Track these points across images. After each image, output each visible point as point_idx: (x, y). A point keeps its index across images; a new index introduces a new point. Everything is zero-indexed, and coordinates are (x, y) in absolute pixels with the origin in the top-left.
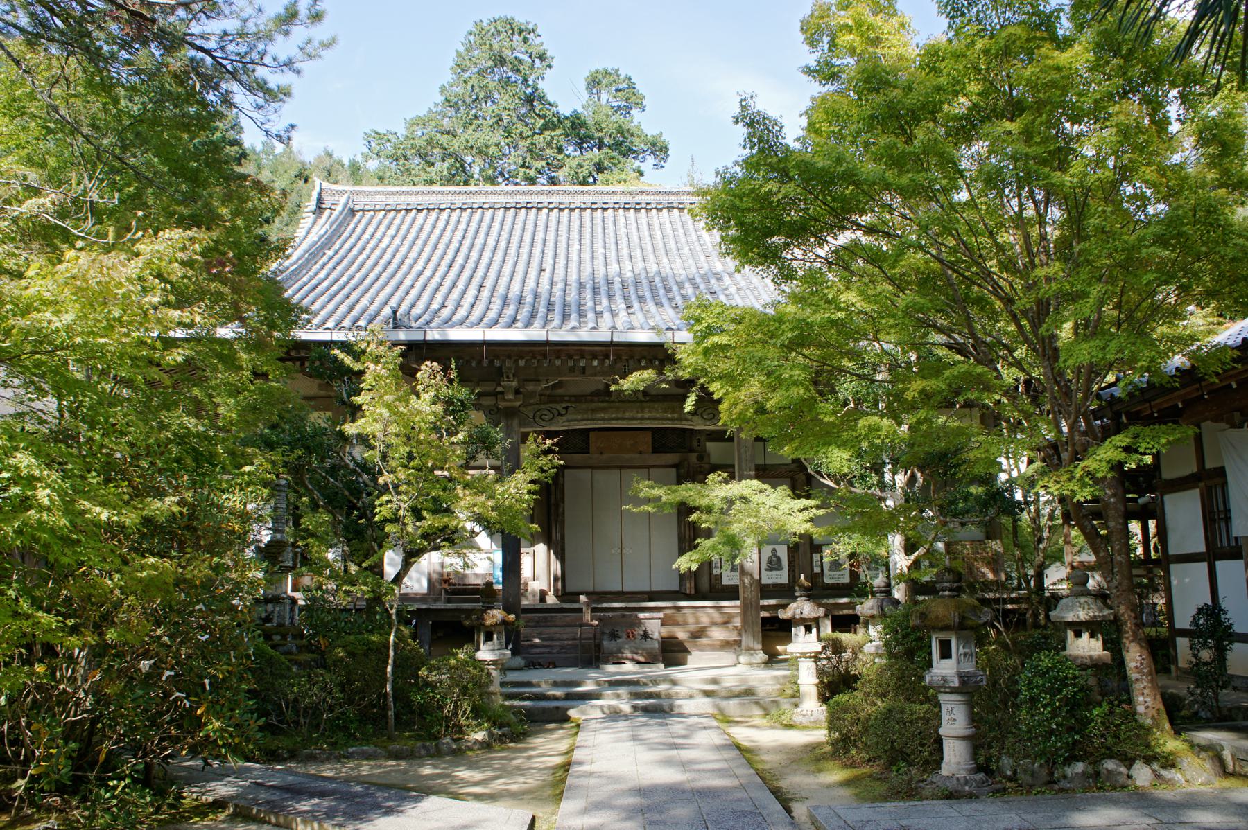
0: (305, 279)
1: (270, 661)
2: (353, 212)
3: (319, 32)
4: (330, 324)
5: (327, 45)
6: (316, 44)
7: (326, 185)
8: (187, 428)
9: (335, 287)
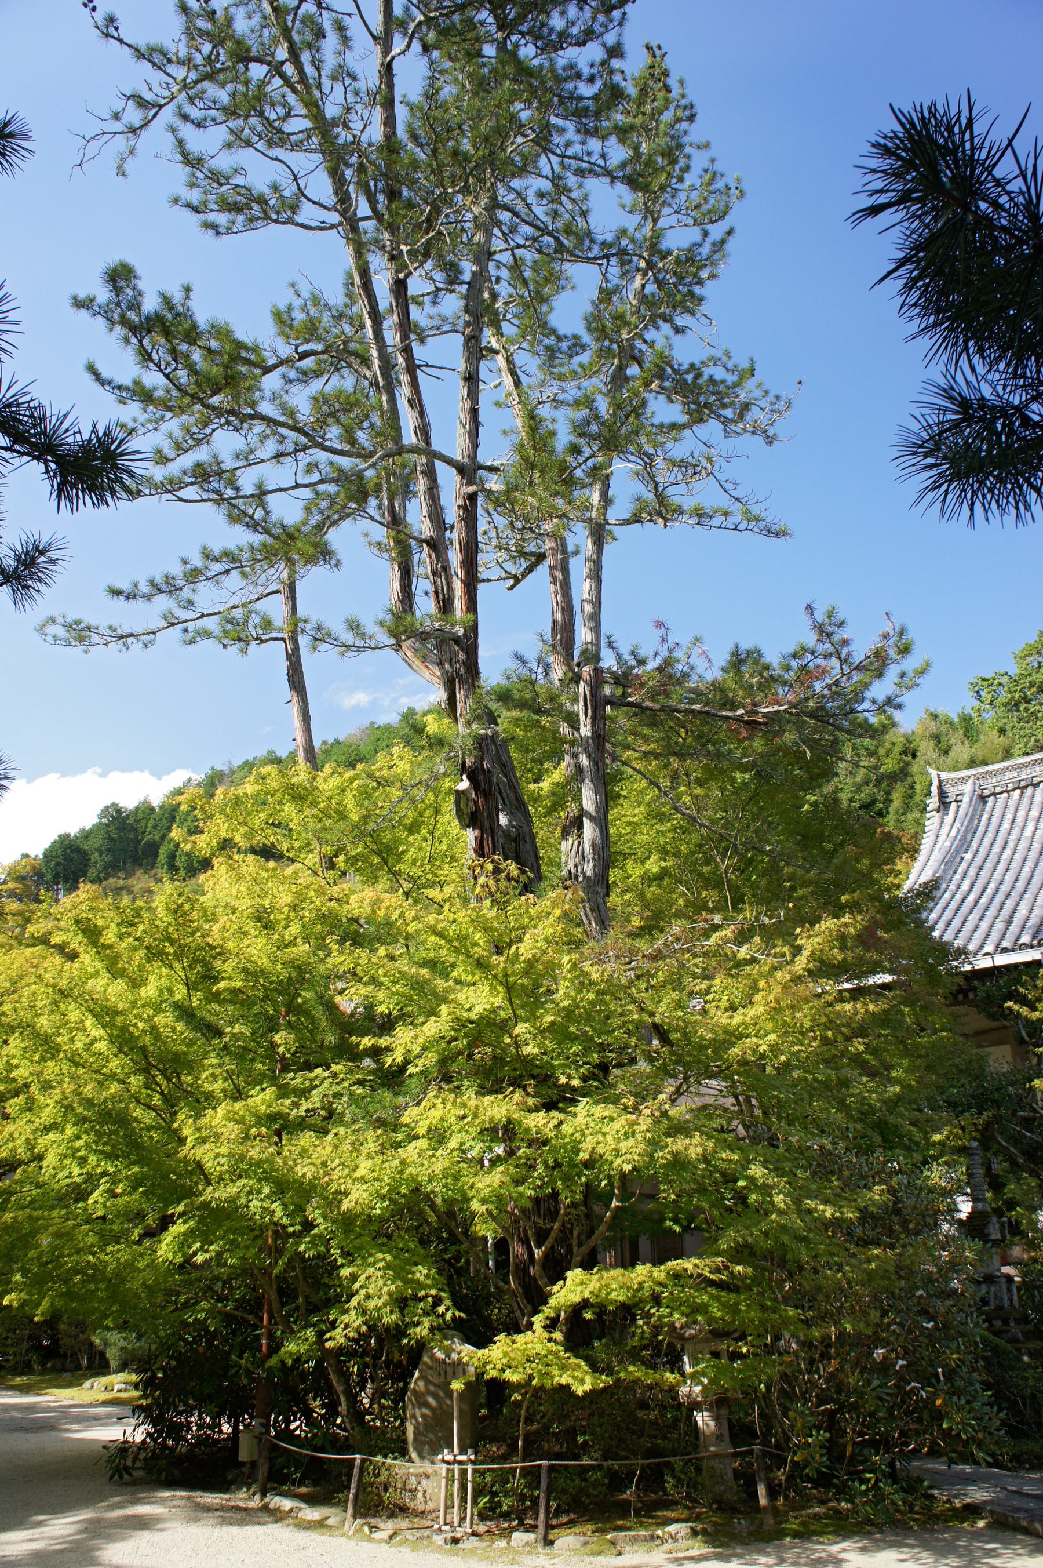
0: (947, 895)
1: (995, 1350)
2: (983, 799)
3: (910, 664)
4: (989, 948)
5: (922, 672)
6: (911, 674)
7: (944, 775)
8: (870, 1105)
9: (984, 900)
